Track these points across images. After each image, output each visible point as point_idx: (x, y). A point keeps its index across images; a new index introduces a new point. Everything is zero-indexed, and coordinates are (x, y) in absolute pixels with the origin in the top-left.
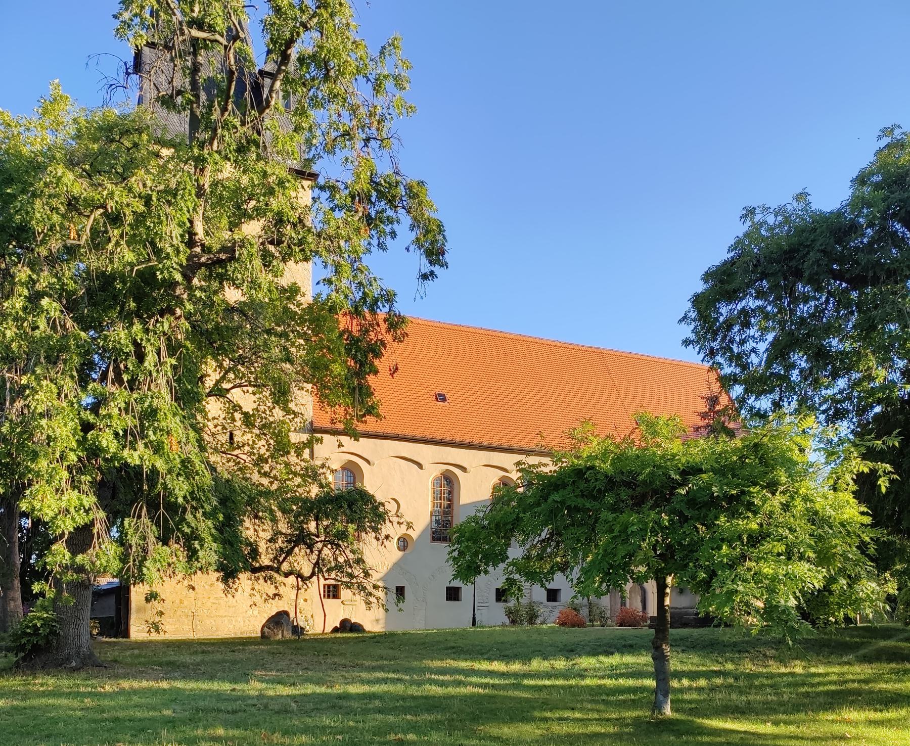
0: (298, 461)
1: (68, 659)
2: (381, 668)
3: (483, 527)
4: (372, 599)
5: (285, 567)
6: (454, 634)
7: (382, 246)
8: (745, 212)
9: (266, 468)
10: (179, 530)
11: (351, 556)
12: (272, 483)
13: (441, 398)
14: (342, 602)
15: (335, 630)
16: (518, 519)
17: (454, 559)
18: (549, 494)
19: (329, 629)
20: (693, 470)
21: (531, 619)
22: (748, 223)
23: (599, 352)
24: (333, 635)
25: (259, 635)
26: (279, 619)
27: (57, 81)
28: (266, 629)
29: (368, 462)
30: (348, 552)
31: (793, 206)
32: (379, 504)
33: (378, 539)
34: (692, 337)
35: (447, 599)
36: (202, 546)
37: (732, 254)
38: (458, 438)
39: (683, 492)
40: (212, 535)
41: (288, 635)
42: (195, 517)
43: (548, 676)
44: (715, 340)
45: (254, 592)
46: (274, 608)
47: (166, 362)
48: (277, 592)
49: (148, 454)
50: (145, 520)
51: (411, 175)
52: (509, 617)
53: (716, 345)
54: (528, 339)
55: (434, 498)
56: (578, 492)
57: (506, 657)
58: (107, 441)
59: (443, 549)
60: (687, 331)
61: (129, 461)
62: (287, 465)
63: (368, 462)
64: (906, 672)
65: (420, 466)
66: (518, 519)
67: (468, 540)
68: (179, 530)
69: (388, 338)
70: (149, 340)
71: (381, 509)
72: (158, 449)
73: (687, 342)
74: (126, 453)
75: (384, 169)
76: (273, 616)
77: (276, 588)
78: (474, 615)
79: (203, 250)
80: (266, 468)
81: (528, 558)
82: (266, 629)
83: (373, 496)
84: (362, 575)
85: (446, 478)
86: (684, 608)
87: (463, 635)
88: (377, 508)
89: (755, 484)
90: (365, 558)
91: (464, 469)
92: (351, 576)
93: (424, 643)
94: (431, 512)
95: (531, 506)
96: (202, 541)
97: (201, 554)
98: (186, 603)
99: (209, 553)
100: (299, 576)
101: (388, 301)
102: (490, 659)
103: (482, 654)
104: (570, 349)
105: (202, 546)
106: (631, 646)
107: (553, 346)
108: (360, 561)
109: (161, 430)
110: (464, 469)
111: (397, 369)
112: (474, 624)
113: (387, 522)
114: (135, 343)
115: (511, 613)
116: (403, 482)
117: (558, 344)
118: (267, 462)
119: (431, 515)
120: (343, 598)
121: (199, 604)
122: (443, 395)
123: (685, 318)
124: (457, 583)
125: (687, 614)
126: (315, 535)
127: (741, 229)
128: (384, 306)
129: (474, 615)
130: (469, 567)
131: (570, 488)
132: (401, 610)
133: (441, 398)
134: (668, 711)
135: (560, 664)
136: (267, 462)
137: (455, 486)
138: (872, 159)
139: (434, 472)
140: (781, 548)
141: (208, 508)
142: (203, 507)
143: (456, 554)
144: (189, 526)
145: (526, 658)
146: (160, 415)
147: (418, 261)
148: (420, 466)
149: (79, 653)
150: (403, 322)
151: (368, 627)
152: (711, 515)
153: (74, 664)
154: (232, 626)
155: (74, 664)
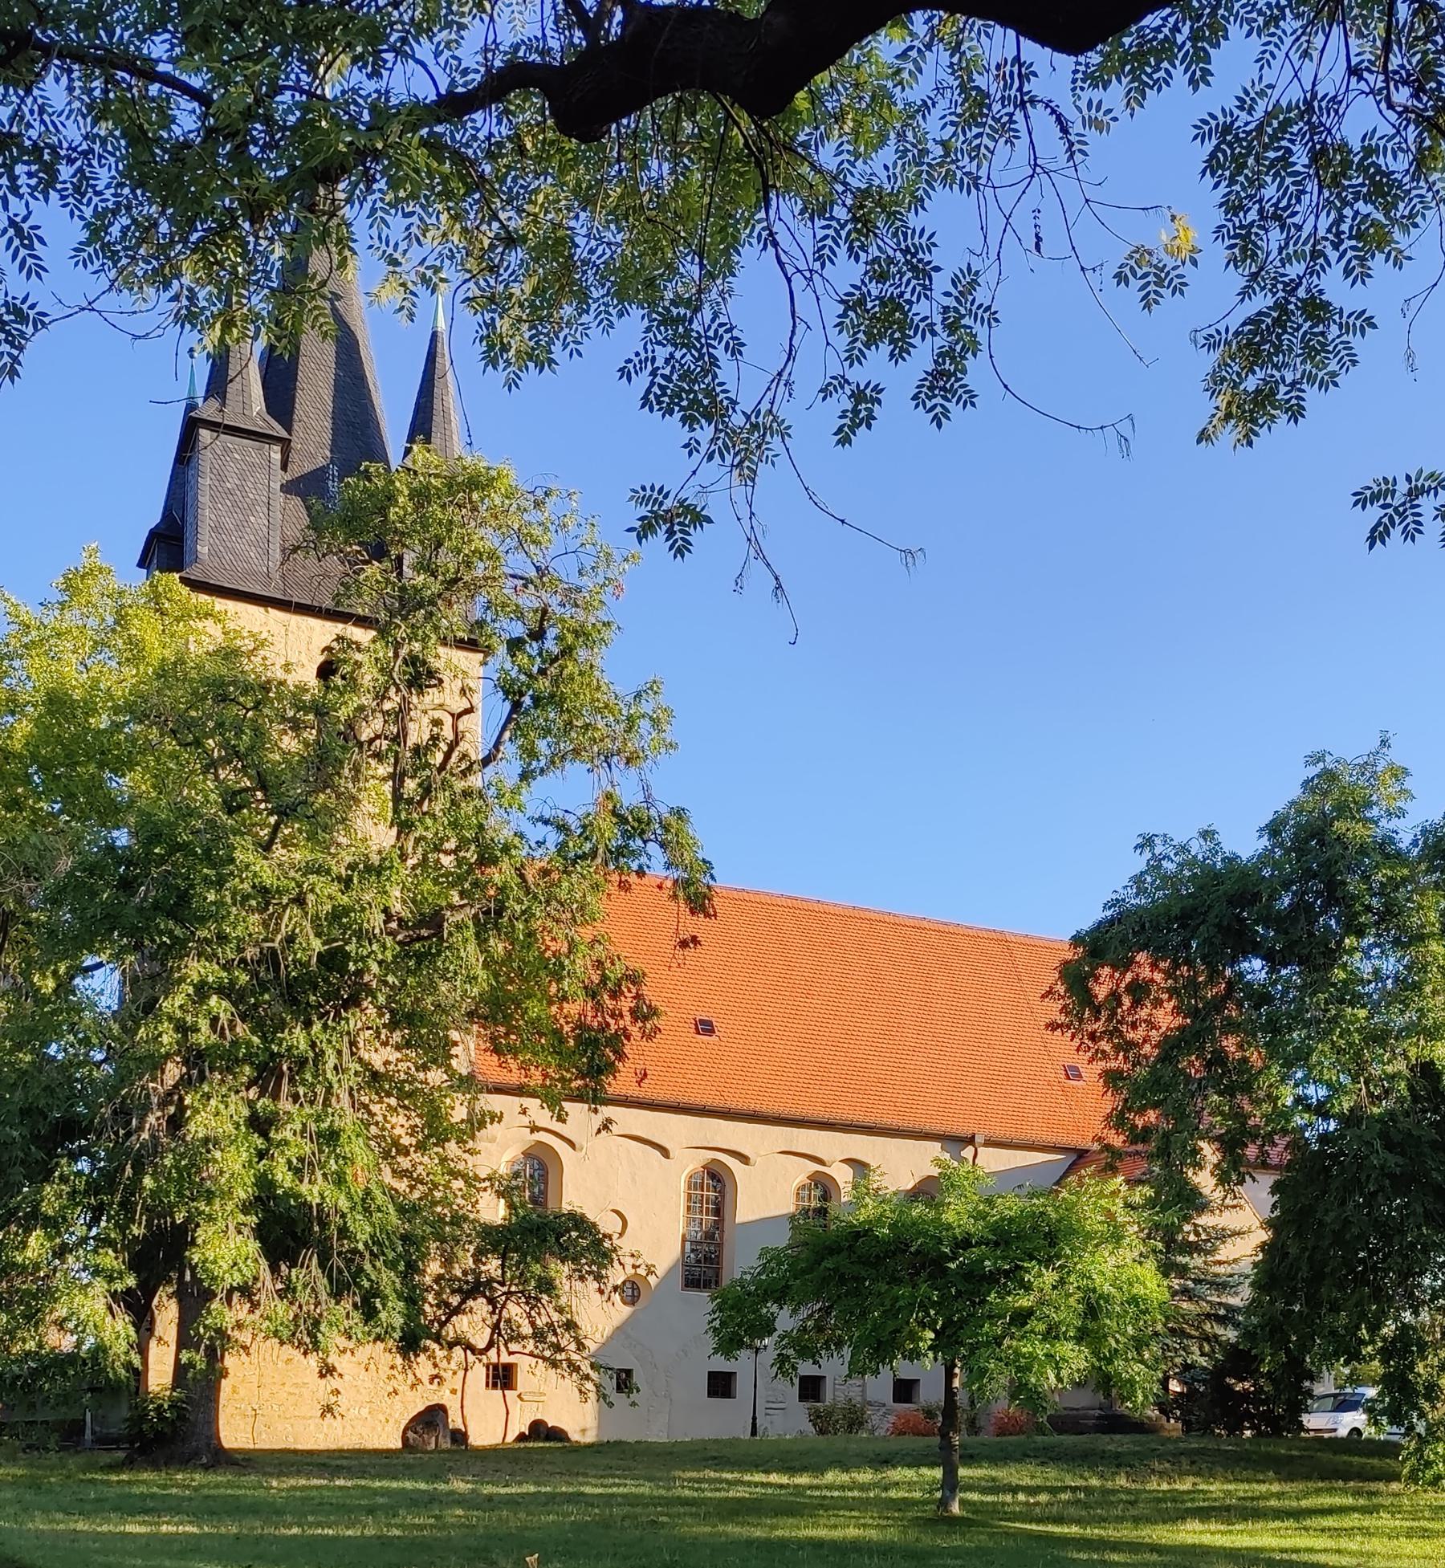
0: (459, 1153)
1: (196, 1454)
2: (613, 1476)
3: (749, 1294)
4: (589, 1386)
5: (449, 1332)
6: (716, 1441)
7: (624, 886)
8: (1140, 840)
9: (404, 1163)
10: (356, 1283)
11: (555, 1316)
12: (412, 1188)
13: (705, 1027)
14: (519, 1396)
15: (521, 1437)
16: (787, 1287)
17: (715, 1329)
18: (823, 1259)
19: (510, 1438)
20: (965, 1243)
21: (850, 1426)
22: (1147, 855)
23: (1002, 941)
24: (517, 1446)
25: (399, 1445)
26: (432, 1418)
27: (94, 546)
28: (410, 1434)
29: (572, 1144)
30: (550, 1310)
31: (1197, 848)
32: (605, 1236)
33: (601, 1292)
34: (1062, 1019)
35: (711, 1394)
36: (384, 1305)
37: (1109, 913)
38: (733, 1103)
39: (953, 1266)
40: (395, 1291)
41: (446, 1444)
42: (374, 1266)
43: (842, 1488)
44: (1098, 1019)
45: (395, 1372)
46: (417, 1404)
47: (348, 1069)
48: (435, 1372)
49: (329, 1190)
50: (315, 1271)
51: (665, 800)
52: (814, 1425)
53: (1098, 1026)
54: (868, 915)
55: (689, 1208)
56: (854, 1258)
57: (791, 1470)
58: (283, 1177)
59: (702, 1299)
60: (1052, 1010)
61: (309, 1199)
62: (443, 1160)
63: (572, 1144)
64: (1438, 1511)
65: (665, 1152)
66: (787, 1287)
67: (732, 1308)
68: (356, 1283)
69: (634, 1030)
70: (329, 1042)
71: (607, 1244)
72: (340, 1180)
73: (1053, 1026)
74: (304, 1188)
75: (629, 797)
76: (420, 1414)
77: (435, 1365)
78: (754, 1419)
79: (399, 925)
80: (404, 1163)
81: (804, 1330)
82: (410, 1434)
83: (594, 1225)
84: (573, 1346)
85: (713, 1176)
86: (1083, 1408)
87: (733, 1442)
88: (600, 1242)
89: (1031, 1258)
90: (576, 1319)
91: (744, 1159)
92: (558, 1348)
93: (671, 1453)
94: (684, 1236)
95: (804, 1272)
96: (384, 1299)
97: (383, 1315)
98: (242, 1392)
99: (393, 1314)
100: (469, 1347)
101: (634, 983)
102: (767, 1472)
103: (757, 1466)
104: (946, 933)
105: (384, 1305)
106: (971, 1457)
107: (916, 929)
108: (570, 1325)
109: (344, 1158)
110: (744, 1159)
111: (645, 1075)
112: (754, 1432)
113: (616, 1264)
114: (313, 1045)
115: (818, 1417)
116: (634, 1180)
117: (925, 924)
118: (407, 1154)
119: (684, 1241)
120: (520, 1389)
121: (266, 1394)
122: (710, 1023)
123: (1050, 992)
124: (720, 1364)
125: (1086, 1417)
126: (499, 1283)
127: (1140, 863)
128: (630, 991)
129: (754, 1419)
130: (731, 1340)
131: (845, 1253)
132: (633, 1404)
133: (705, 1027)
134: (956, 1509)
135: (865, 1476)
136: (407, 1154)
137: (728, 1189)
138: (1295, 792)
139: (689, 1163)
140: (1042, 1327)
141: (391, 1255)
142: (384, 1254)
143: (717, 1323)
144: (369, 1280)
145: (819, 1469)
146: (343, 1138)
147: (675, 917)
148: (665, 1152)
149: (209, 1445)
150: (655, 1014)
151: (575, 1436)
152: (983, 1290)
153: (204, 1460)
154: (321, 1436)
155: (204, 1460)
